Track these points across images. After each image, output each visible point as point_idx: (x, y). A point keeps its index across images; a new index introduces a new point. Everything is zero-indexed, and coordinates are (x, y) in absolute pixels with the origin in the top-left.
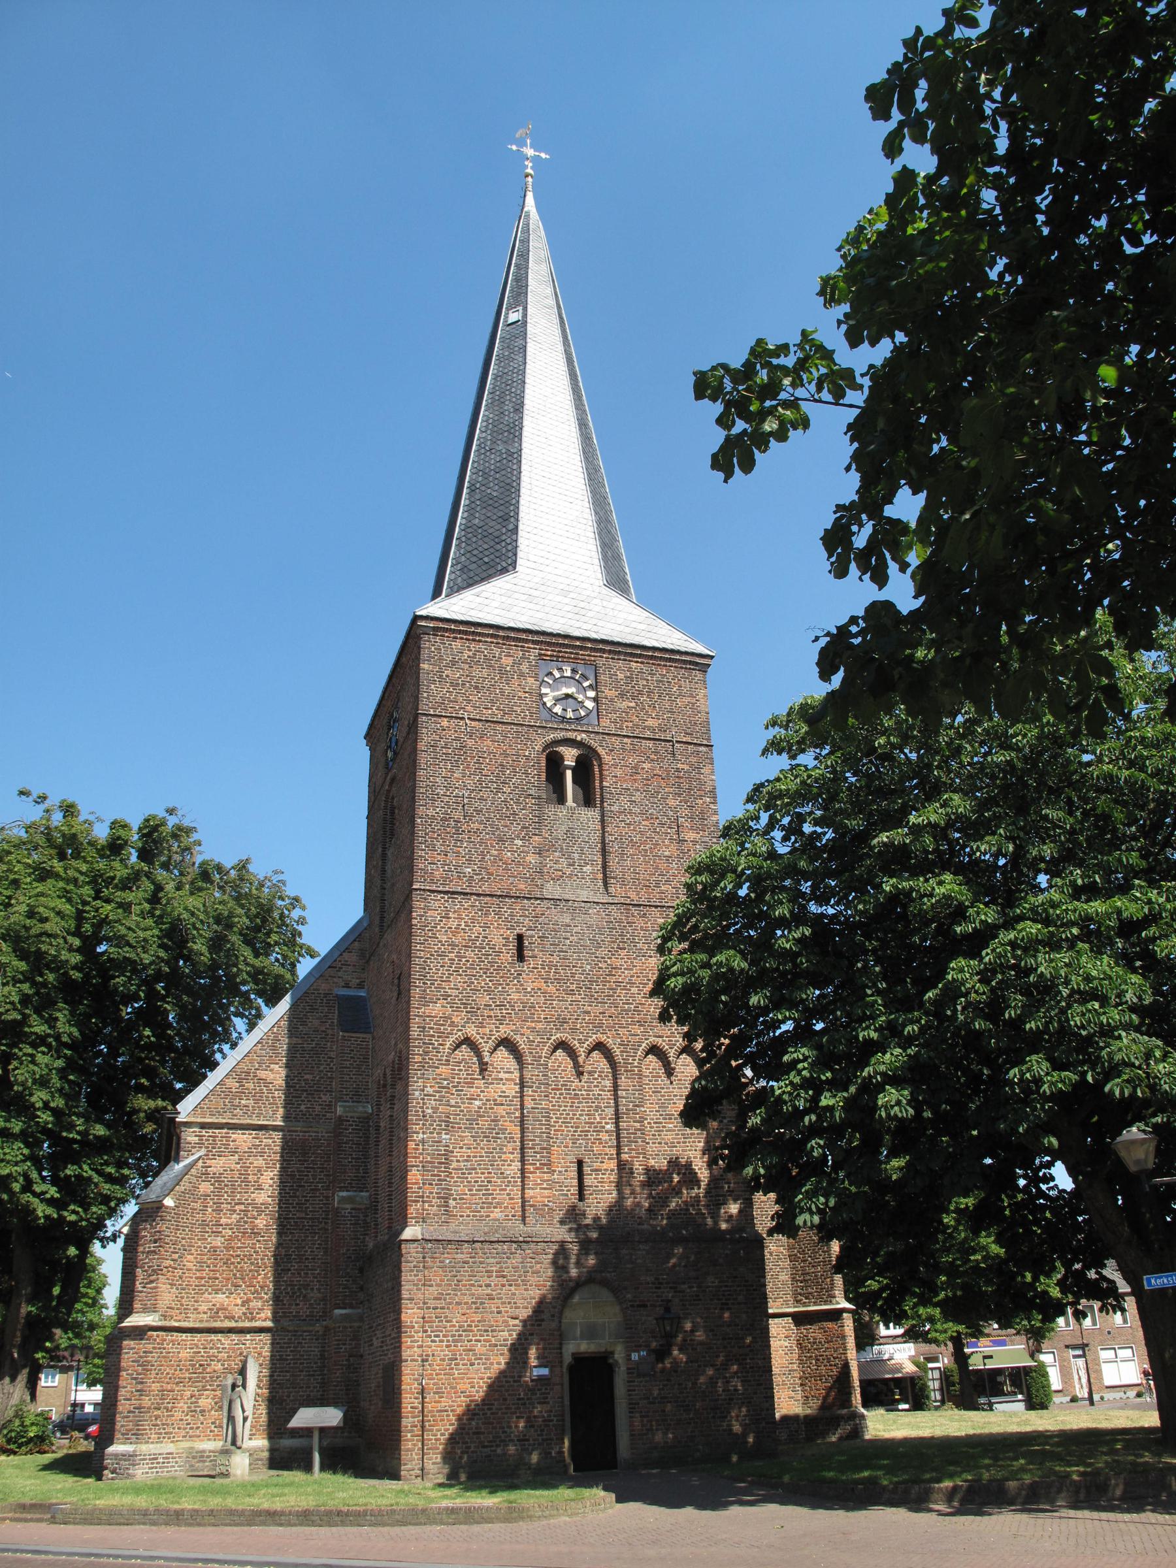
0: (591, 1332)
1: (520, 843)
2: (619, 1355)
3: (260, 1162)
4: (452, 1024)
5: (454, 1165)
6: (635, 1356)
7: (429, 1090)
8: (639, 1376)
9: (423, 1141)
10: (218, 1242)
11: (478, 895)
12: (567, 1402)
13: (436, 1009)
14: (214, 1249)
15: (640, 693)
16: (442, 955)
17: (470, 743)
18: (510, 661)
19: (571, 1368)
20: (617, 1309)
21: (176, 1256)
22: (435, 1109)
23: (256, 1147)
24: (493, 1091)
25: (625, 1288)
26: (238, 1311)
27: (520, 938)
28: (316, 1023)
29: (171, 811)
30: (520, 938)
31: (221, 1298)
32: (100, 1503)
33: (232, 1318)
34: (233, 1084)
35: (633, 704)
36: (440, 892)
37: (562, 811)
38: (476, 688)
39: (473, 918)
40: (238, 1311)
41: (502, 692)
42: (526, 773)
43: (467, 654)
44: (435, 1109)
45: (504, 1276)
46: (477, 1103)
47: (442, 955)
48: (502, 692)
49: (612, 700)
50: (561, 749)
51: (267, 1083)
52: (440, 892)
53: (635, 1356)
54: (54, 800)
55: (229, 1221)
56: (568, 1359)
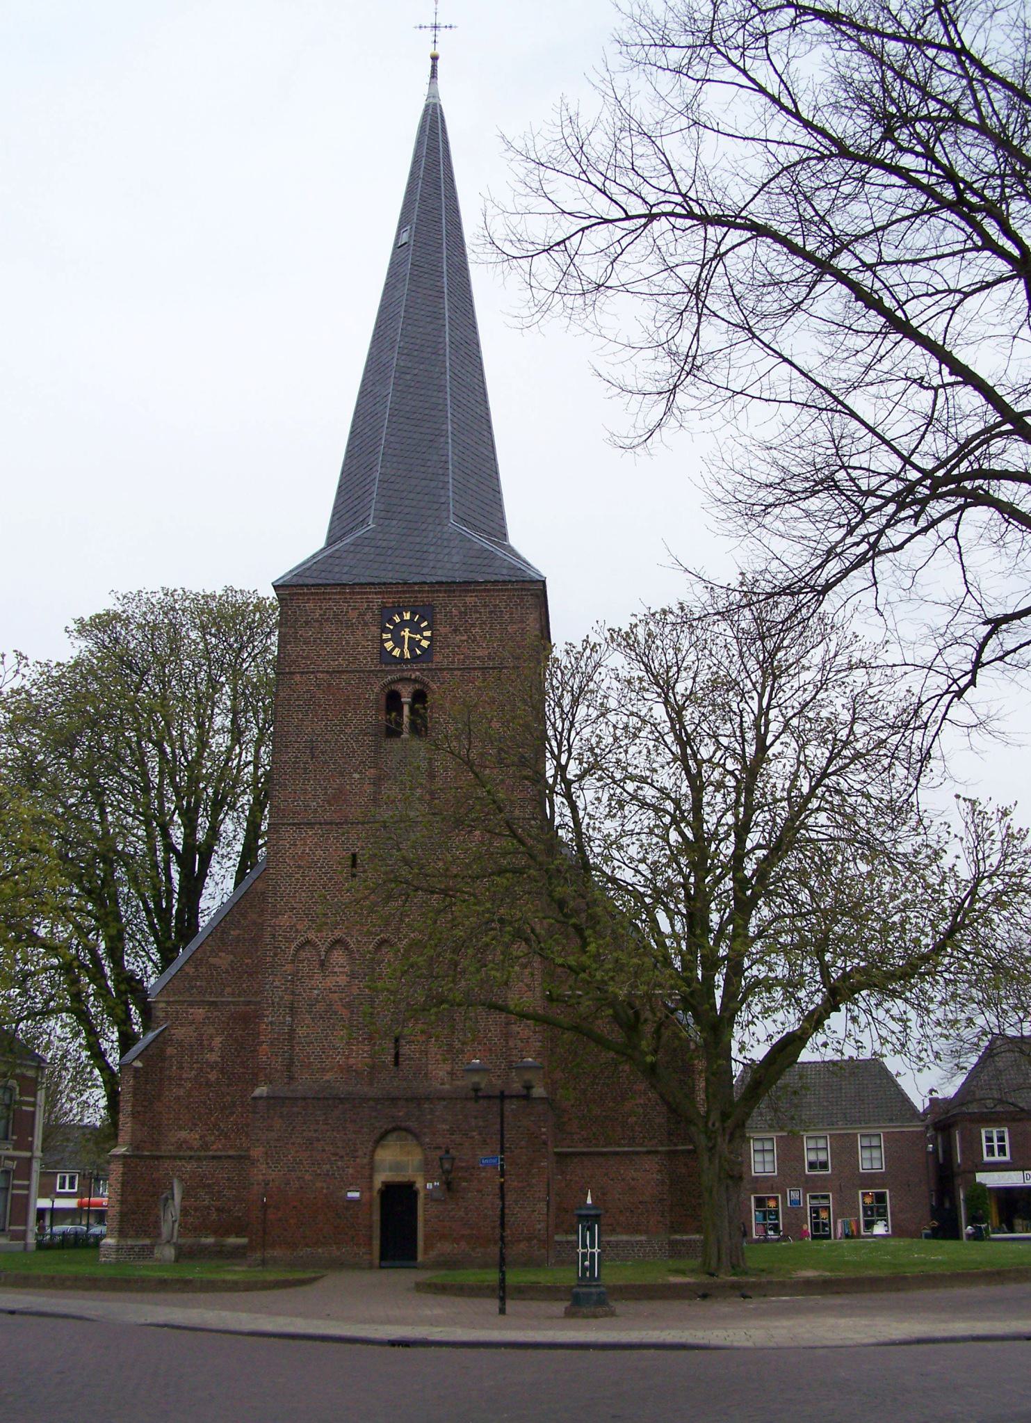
0: (397, 1167)
2: (419, 1185)
3: (211, 1030)
4: (297, 931)
6: (429, 1186)
7: (277, 983)
9: (271, 1023)
10: (181, 1092)
13: (284, 920)
14: (178, 1098)
15: (473, 625)
16: (290, 876)
20: (419, 1150)
21: (146, 1103)
23: (208, 1018)
24: (330, 982)
26: (196, 1144)
27: (354, 855)
28: (255, 916)
30: (354, 855)
31: (184, 1134)
32: (137, 1273)
33: (191, 1149)
34: (190, 970)
35: (465, 638)
37: (396, 744)
38: (326, 643)
40: (196, 1144)
41: (347, 643)
47: (290, 876)
48: (347, 643)
49: (446, 636)
50: (399, 687)
51: (216, 967)
53: (429, 1186)
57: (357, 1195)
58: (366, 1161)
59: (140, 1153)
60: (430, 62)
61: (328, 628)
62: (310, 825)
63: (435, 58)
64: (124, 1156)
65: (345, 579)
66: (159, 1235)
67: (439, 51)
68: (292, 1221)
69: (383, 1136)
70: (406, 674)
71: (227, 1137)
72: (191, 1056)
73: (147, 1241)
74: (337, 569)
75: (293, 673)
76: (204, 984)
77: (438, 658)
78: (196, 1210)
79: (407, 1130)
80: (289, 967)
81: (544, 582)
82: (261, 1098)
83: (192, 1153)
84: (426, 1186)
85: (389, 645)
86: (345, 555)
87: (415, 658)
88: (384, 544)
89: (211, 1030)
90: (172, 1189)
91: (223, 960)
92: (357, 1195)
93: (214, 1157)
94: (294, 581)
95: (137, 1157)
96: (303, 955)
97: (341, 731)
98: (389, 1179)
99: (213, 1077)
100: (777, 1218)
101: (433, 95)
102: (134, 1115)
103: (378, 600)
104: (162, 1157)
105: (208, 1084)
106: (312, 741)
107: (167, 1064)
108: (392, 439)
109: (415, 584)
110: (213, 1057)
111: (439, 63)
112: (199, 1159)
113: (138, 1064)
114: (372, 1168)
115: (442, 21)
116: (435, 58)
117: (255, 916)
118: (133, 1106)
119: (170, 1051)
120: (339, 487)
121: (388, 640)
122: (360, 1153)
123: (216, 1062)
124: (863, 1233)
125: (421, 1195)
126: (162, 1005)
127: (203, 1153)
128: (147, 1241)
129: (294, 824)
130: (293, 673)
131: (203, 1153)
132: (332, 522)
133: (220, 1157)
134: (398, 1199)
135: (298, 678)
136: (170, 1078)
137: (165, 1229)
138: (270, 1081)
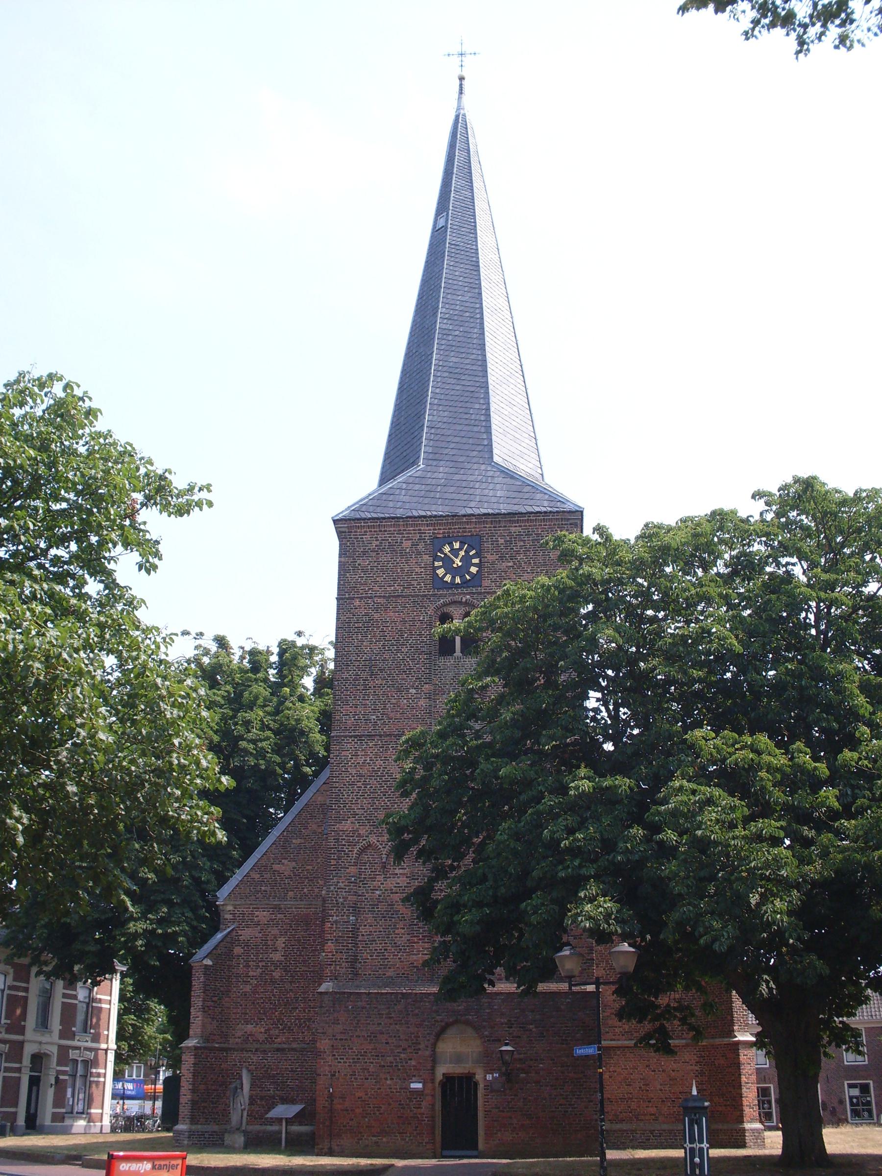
0: (458, 1059)
1: (414, 691)
2: (479, 1077)
3: (275, 931)
4: (359, 836)
5: (360, 938)
6: (489, 1077)
8: (492, 1091)
9: (336, 922)
10: (248, 988)
11: (380, 736)
12: (438, 1106)
13: (347, 825)
15: (518, 552)
17: (376, 616)
18: (409, 543)
19: (443, 1084)
20: (478, 1042)
21: (215, 999)
22: (345, 898)
23: (272, 920)
25: (484, 1027)
26: (262, 1038)
28: (314, 827)
29: (299, 634)
35: (510, 564)
36: (351, 737)
37: (450, 661)
39: (376, 755)
40: (262, 1038)
41: (402, 571)
42: (420, 635)
43: (375, 543)
44: (345, 898)
45: (390, 1018)
46: (378, 892)
48: (402, 571)
49: (493, 563)
52: (351, 737)
53: (489, 1077)
54: (209, 635)
55: (255, 974)
56: (439, 1077)
57: (420, 1086)
58: (427, 1053)
59: (209, 1045)
60: (458, 82)
61: (383, 558)
62: (371, 737)
63: (461, 79)
64: (196, 1048)
65: (399, 513)
66: (229, 1121)
67: (464, 74)
68: (357, 1111)
69: (443, 1030)
70: (457, 598)
71: (290, 1030)
72: (257, 955)
73: (216, 1128)
74: (391, 504)
75: (353, 598)
76: (268, 889)
77: (486, 583)
78: (262, 1098)
79: (468, 1023)
80: (353, 870)
81: (582, 512)
82: (326, 993)
83: (258, 1046)
84: (485, 1077)
85: (441, 572)
86: (398, 492)
87: (465, 583)
88: (434, 482)
89: (275, 931)
90: (241, 1078)
91: (286, 867)
92: (420, 1086)
93: (278, 1050)
94: (353, 515)
95: (205, 1048)
96: (365, 858)
97: (398, 651)
98: (451, 1071)
99: (277, 974)
100: (770, 1108)
101: (459, 108)
102: (204, 1009)
103: (429, 531)
104: (230, 1049)
105: (273, 981)
106: (370, 660)
107: (234, 963)
108: (438, 391)
109: (465, 516)
110: (277, 957)
111: (464, 82)
112: (264, 1052)
113: (208, 962)
114: (434, 1060)
115: (467, 49)
116: (461, 79)
117: (314, 827)
118: (204, 1001)
119: (238, 950)
120: (389, 436)
121: (439, 567)
122: (422, 1046)
123: (280, 962)
124: (849, 1120)
125: (481, 1086)
126: (230, 908)
127: (268, 1046)
128: (216, 1128)
129: (355, 737)
130: (353, 598)
131: (268, 1046)
132: (383, 467)
133: (283, 1050)
134: (458, 1091)
135: (357, 603)
136: (238, 976)
137: (235, 1118)
138: (335, 977)
